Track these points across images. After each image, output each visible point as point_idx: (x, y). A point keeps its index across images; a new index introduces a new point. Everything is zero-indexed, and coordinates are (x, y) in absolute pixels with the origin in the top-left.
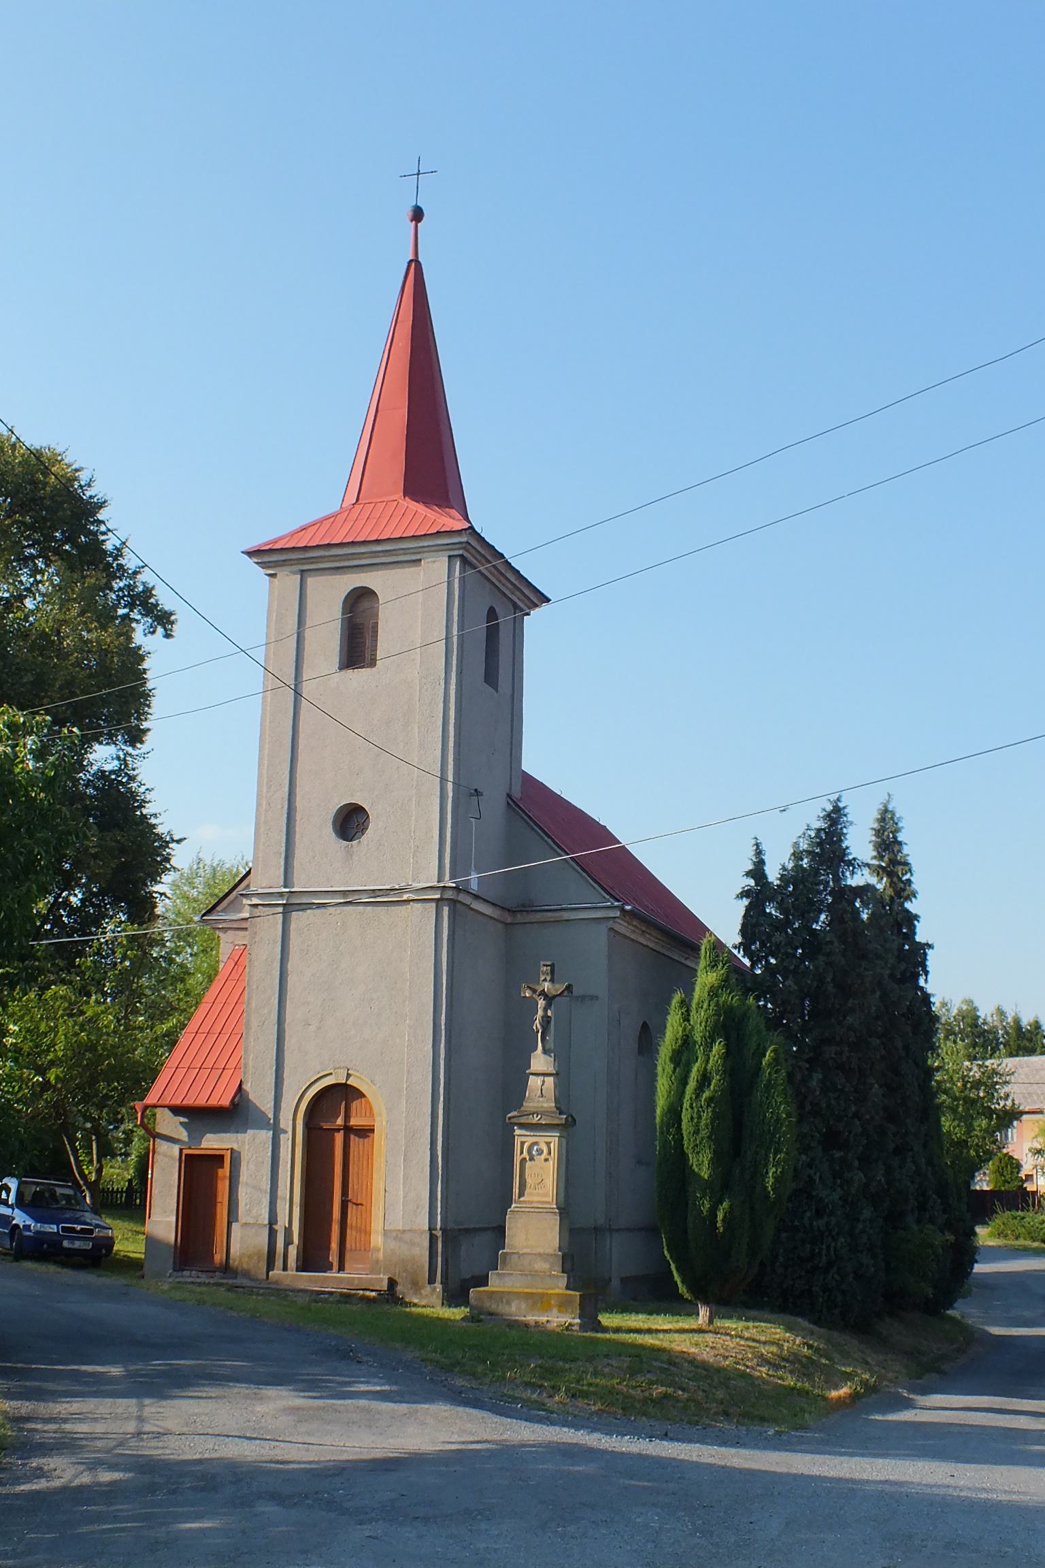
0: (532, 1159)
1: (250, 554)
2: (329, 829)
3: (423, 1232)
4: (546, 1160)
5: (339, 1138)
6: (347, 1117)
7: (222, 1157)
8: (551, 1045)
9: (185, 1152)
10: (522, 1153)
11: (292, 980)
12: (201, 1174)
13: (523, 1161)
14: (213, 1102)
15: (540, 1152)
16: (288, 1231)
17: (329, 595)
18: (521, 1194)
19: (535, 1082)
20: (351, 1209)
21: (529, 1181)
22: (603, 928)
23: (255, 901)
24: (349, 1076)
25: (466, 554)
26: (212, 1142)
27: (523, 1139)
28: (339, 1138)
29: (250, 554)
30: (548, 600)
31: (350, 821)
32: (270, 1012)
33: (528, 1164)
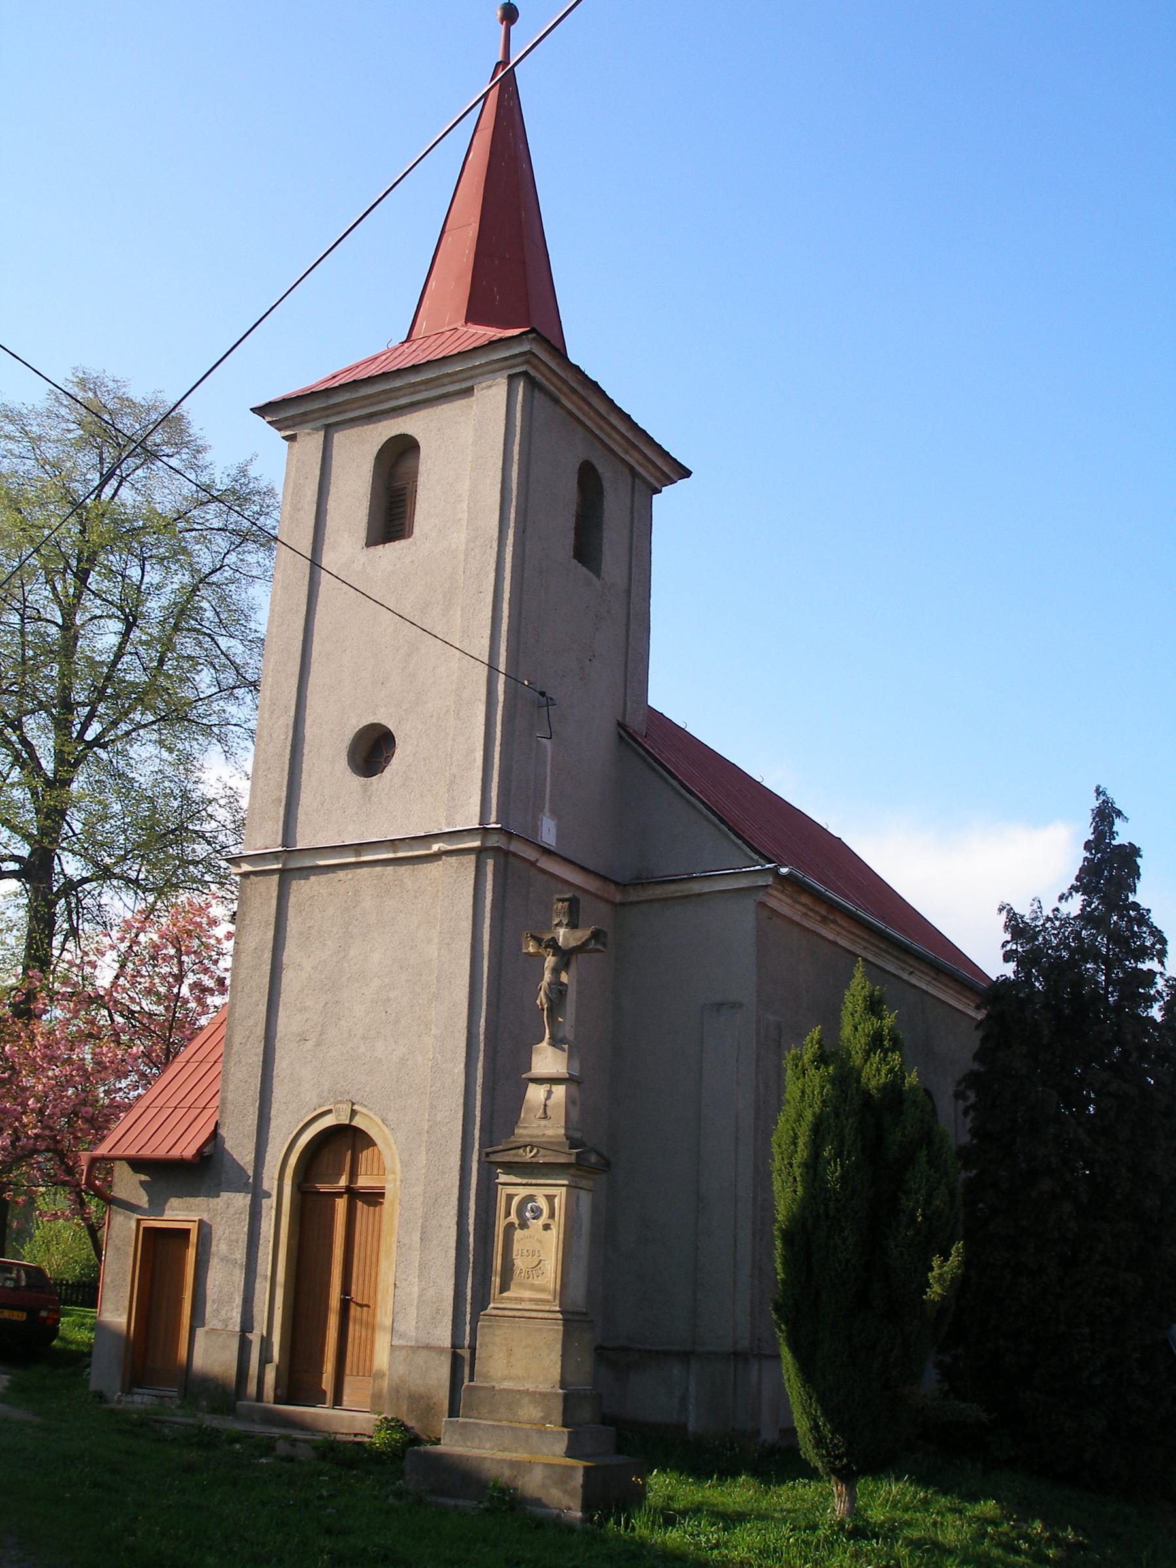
0: (524, 1225)
1: (260, 411)
2: (343, 762)
3: (440, 1350)
4: (547, 1227)
5: (341, 1204)
6: (353, 1175)
7: (187, 1232)
8: (568, 1031)
9: (144, 1224)
10: (508, 1214)
11: (288, 977)
12: (162, 1251)
13: (510, 1228)
14: (176, 1153)
15: (537, 1213)
16: (266, 1342)
17: (358, 452)
18: (504, 1287)
19: (535, 1094)
20: (354, 1311)
21: (519, 1263)
22: (749, 904)
23: (246, 868)
24: (353, 1113)
25: (532, 372)
26: (180, 1213)
27: (511, 1190)
28: (341, 1204)
29: (260, 411)
30: (686, 473)
31: (373, 750)
32: (256, 1025)
33: (518, 1234)
